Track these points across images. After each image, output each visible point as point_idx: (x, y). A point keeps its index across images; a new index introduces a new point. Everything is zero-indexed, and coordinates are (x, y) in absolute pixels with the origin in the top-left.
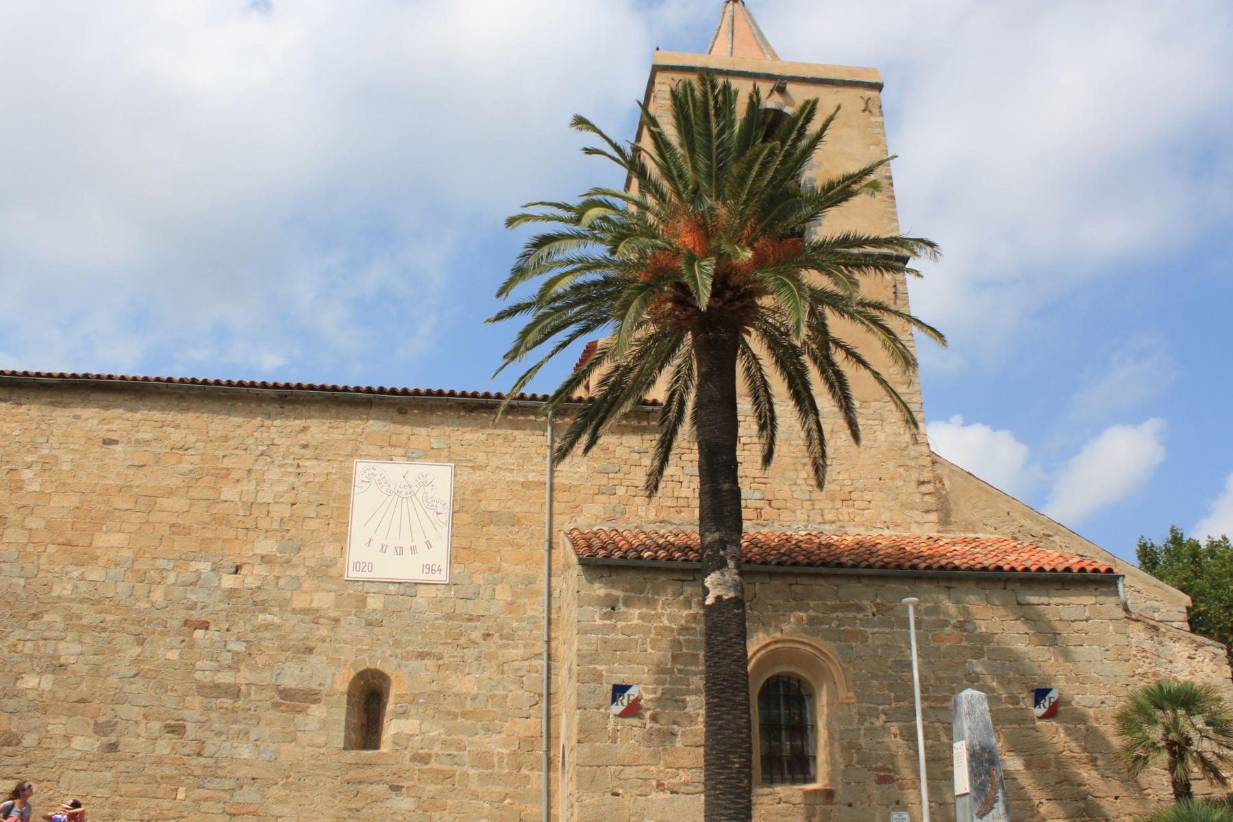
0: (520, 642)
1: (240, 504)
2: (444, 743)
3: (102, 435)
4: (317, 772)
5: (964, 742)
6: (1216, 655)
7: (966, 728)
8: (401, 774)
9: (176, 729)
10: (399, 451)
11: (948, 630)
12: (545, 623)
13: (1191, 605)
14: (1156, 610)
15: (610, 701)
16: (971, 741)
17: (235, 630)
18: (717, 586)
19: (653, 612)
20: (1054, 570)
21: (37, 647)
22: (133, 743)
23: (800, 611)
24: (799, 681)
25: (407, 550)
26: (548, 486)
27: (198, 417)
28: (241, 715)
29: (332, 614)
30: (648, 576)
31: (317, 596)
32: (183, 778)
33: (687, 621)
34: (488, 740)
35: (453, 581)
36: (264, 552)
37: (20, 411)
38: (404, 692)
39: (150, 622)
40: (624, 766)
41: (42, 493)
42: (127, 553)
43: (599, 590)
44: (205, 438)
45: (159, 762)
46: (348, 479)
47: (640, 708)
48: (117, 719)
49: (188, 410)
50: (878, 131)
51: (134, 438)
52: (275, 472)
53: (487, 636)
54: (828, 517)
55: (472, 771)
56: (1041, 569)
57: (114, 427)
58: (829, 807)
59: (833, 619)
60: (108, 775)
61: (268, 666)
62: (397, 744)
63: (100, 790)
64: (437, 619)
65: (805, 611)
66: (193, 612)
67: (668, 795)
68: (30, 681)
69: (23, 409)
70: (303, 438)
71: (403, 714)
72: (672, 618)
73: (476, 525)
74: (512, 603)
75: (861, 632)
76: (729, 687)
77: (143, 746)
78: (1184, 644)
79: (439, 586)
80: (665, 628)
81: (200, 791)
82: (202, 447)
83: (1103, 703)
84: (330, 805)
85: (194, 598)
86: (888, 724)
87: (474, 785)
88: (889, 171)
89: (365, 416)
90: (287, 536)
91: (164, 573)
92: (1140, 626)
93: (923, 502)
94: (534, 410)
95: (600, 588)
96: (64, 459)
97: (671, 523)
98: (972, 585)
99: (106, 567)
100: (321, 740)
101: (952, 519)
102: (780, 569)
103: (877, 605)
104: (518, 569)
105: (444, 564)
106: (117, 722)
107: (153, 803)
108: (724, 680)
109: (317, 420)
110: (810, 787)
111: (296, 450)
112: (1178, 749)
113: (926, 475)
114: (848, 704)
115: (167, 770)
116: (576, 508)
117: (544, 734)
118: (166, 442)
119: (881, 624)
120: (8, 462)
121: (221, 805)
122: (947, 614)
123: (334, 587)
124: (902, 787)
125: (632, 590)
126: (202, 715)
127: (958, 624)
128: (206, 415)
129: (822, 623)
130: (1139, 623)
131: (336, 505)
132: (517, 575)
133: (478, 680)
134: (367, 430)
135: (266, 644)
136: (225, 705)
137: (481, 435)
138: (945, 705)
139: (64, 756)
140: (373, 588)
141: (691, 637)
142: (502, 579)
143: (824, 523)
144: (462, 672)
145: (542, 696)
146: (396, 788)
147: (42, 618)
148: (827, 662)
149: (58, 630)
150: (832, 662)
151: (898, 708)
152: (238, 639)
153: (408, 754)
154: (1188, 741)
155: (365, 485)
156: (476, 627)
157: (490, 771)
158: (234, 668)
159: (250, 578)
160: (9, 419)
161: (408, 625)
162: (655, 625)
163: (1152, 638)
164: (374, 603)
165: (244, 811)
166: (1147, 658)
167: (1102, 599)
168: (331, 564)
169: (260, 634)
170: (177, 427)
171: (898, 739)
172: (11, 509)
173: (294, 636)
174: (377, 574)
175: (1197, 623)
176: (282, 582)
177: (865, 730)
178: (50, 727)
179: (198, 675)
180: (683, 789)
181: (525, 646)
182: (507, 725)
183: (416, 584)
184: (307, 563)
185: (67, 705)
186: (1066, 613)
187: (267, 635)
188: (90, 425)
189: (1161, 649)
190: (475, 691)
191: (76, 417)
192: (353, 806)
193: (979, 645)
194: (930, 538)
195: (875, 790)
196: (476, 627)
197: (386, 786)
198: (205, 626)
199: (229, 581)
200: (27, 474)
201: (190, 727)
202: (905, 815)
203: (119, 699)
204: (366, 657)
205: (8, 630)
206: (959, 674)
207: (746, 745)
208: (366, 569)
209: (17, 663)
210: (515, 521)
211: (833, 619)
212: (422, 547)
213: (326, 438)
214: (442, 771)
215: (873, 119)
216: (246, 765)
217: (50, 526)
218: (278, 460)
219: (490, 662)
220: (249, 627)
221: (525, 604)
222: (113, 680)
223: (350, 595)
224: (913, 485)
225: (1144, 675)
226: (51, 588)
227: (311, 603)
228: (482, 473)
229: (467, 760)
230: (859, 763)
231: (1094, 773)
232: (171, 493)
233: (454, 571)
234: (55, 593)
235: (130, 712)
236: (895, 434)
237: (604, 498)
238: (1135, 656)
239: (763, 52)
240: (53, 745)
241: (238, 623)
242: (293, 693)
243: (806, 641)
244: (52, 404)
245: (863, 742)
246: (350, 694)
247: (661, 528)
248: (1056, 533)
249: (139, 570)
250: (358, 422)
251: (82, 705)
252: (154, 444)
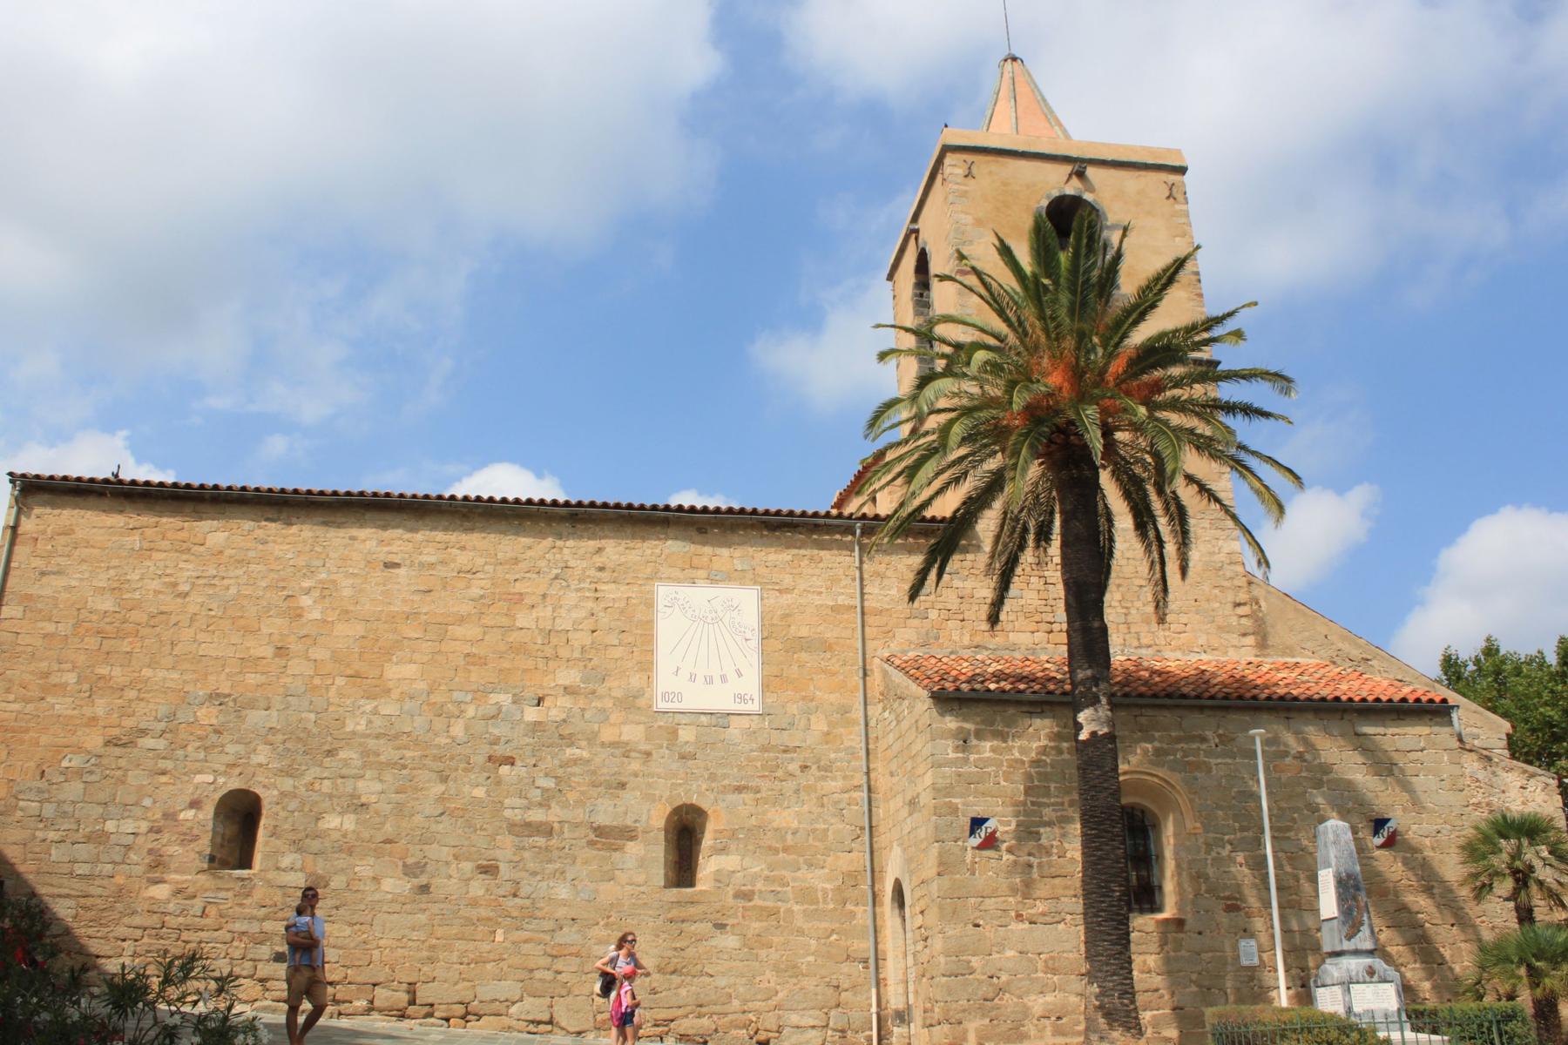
0: (839, 773)
1: (537, 631)
2: (767, 879)
3: (382, 557)
4: (638, 911)
5: (1331, 870)
6: (1547, 785)
7: (1332, 856)
8: (724, 912)
9: (489, 870)
10: (702, 573)
11: (1288, 760)
12: (863, 753)
13: (1511, 731)
14: (1476, 737)
15: (968, 833)
16: (1338, 870)
17: (542, 766)
18: (1090, 721)
19: (1004, 745)
20: (1390, 700)
21: (335, 786)
22: (444, 884)
23: (1145, 742)
24: (1143, 812)
25: (717, 680)
26: (859, 609)
27: (484, 538)
28: (556, 853)
29: (644, 747)
30: (996, 708)
31: (625, 729)
32: (500, 920)
33: (1037, 754)
34: (811, 875)
35: (767, 711)
36: (567, 683)
37: (291, 532)
38: (722, 827)
39: (452, 759)
40: (983, 897)
41: (325, 621)
42: (422, 686)
43: (951, 723)
44: (493, 560)
45: (474, 903)
46: (650, 604)
47: (996, 840)
48: (426, 860)
49: (472, 530)
50: (1183, 220)
51: (417, 561)
52: (571, 598)
53: (804, 768)
54: (1144, 641)
55: (796, 908)
56: (1378, 700)
57: (394, 548)
58: (1181, 935)
59: (1178, 750)
60: (422, 918)
61: (580, 803)
62: (719, 881)
63: (415, 933)
64: (752, 751)
65: (1151, 743)
66: (496, 747)
67: (1027, 925)
68: (332, 822)
69: (294, 529)
70: (599, 560)
71: (723, 850)
72: (1023, 750)
73: (786, 651)
74: (828, 734)
75: (1205, 762)
76: (1108, 819)
77: (456, 887)
78: (1516, 774)
79: (752, 717)
80: (1016, 761)
81: (520, 932)
82: (491, 570)
83: (1438, 832)
84: (654, 944)
85: (496, 732)
86: (1234, 854)
87: (799, 922)
88: (1196, 265)
89: (663, 536)
90: (590, 665)
91: (463, 706)
92: (1474, 756)
93: (1239, 624)
94: (849, 530)
95: (951, 722)
96: (343, 585)
97: (986, 649)
98: (1310, 716)
99: (400, 700)
100: (641, 878)
101: (1270, 643)
102: (1127, 701)
103: (1219, 736)
104: (833, 698)
105: (756, 695)
106: (426, 864)
107: (471, 946)
108: (1102, 813)
109: (612, 541)
110: (1160, 916)
111: (592, 572)
112: (1523, 877)
113: (1242, 597)
114: (1195, 834)
115: (484, 912)
116: (888, 633)
117: (868, 869)
118: (452, 565)
119: (1224, 755)
120: (284, 588)
121: (542, 946)
122: (1286, 745)
123: (643, 719)
124: (1248, 915)
125: (983, 722)
126: (515, 854)
127: (1298, 755)
128: (492, 536)
129: (1168, 754)
130: (1473, 754)
131: (639, 632)
132: (831, 704)
133: (798, 814)
134: (666, 551)
135: (576, 780)
136: (538, 844)
137: (786, 556)
138: (1287, 835)
139: (376, 899)
140: (685, 719)
141: (1042, 770)
142: (817, 708)
143: (1140, 647)
144: (781, 805)
145: (864, 829)
146: (721, 926)
147: (337, 754)
148: (1173, 792)
149: (355, 768)
150: (1178, 792)
151: (1243, 838)
152: (546, 775)
153: (730, 891)
154: (1531, 868)
155: (669, 611)
156: (792, 759)
157: (814, 907)
158: (545, 806)
159: (556, 709)
160: (280, 540)
161: (723, 758)
162: (1007, 757)
163: (1486, 769)
164: (686, 735)
165: (566, 952)
166: (1481, 788)
167: (1436, 729)
168: (637, 696)
169: (569, 769)
170: (463, 548)
171: (1244, 868)
172: (292, 639)
173: (605, 770)
174: (689, 704)
175: (1517, 749)
176: (588, 715)
177: (1213, 859)
178: (357, 869)
179: (508, 813)
180: (1041, 919)
181: (845, 778)
182: (830, 859)
183: (728, 714)
184: (613, 694)
185: (373, 846)
186: (1401, 743)
187: (576, 770)
188: (368, 547)
189: (1494, 779)
190: (795, 825)
191: (353, 538)
192: (678, 945)
193: (1318, 776)
194: (1250, 663)
195: (1224, 919)
196: (792, 759)
197: (710, 925)
198: (511, 761)
199: (531, 714)
200: (306, 601)
201: (503, 867)
202: (1253, 942)
203: (425, 840)
204: (681, 790)
205: (304, 768)
206: (1300, 804)
207: (1125, 875)
208: (675, 699)
209: (317, 802)
210: (827, 647)
211: (1178, 750)
212: (732, 676)
213: (623, 559)
214: (767, 908)
215: (1178, 207)
216: (565, 905)
217: (336, 658)
218: (574, 584)
219: (809, 795)
220: (556, 762)
221: (841, 735)
222: (418, 819)
223: (660, 727)
224: (1229, 606)
225: (1478, 805)
226: (344, 723)
227: (620, 736)
228: (789, 596)
229: (791, 896)
230: (1207, 892)
231: (1429, 901)
232: (462, 620)
233: (767, 700)
234: (348, 729)
235: (437, 852)
236: (1210, 553)
237: (916, 622)
238: (1469, 786)
239: (1050, 123)
240: (362, 888)
241: (545, 758)
242: (607, 830)
243: (1154, 772)
244: (325, 524)
245: (1210, 871)
246: (666, 831)
247: (976, 653)
248: (1375, 657)
249: (435, 703)
250: (657, 542)
251: (388, 846)
252: (439, 567)
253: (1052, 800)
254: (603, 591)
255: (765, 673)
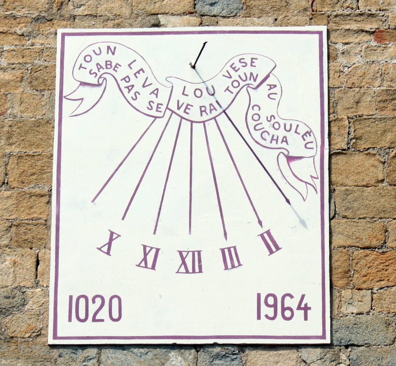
35: (342, 335)
79: (304, 353)
131: (15, 150)
183: (242, 347)
208: (104, 314)
255: (338, 240)
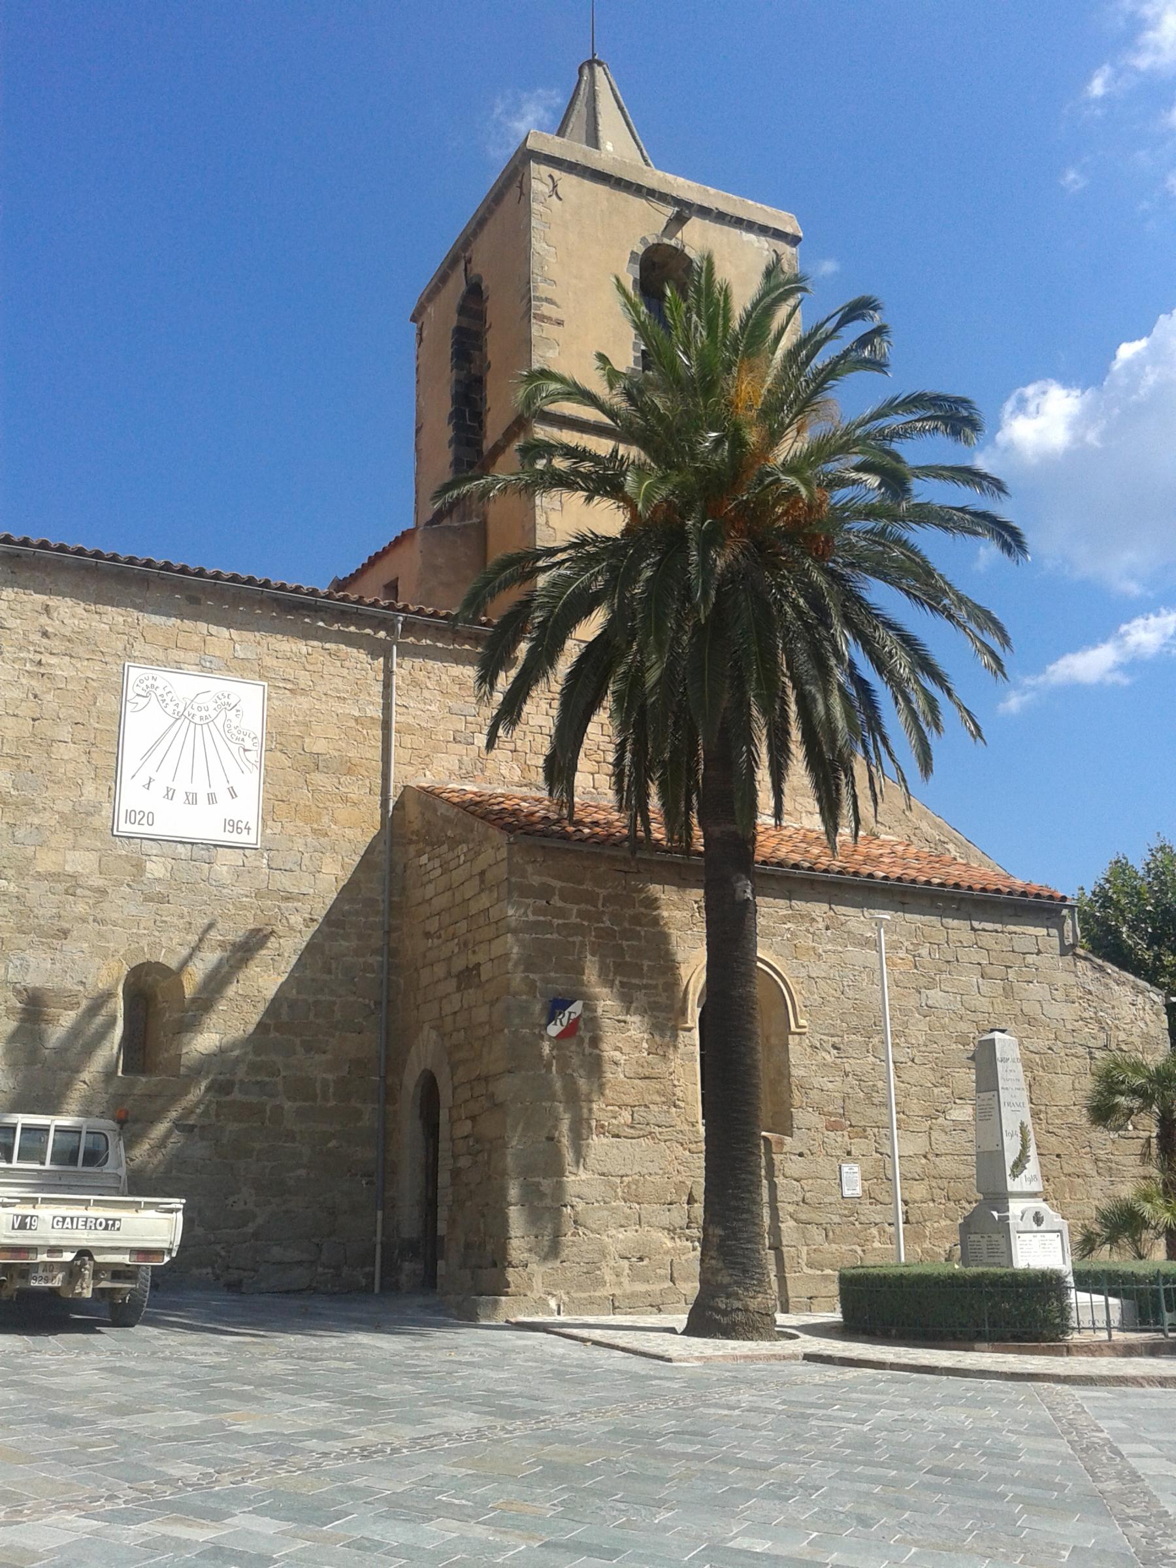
10: (192, 657)
25: (202, 799)
29: (97, 881)
31: (70, 855)
46: (120, 691)
55: (288, 1105)
79: (247, 852)
111: (36, 637)
164: (155, 869)
174: (160, 829)
176: (20, 834)
208: (144, 821)
212: (223, 795)
253: (645, 981)
254: (51, 665)
